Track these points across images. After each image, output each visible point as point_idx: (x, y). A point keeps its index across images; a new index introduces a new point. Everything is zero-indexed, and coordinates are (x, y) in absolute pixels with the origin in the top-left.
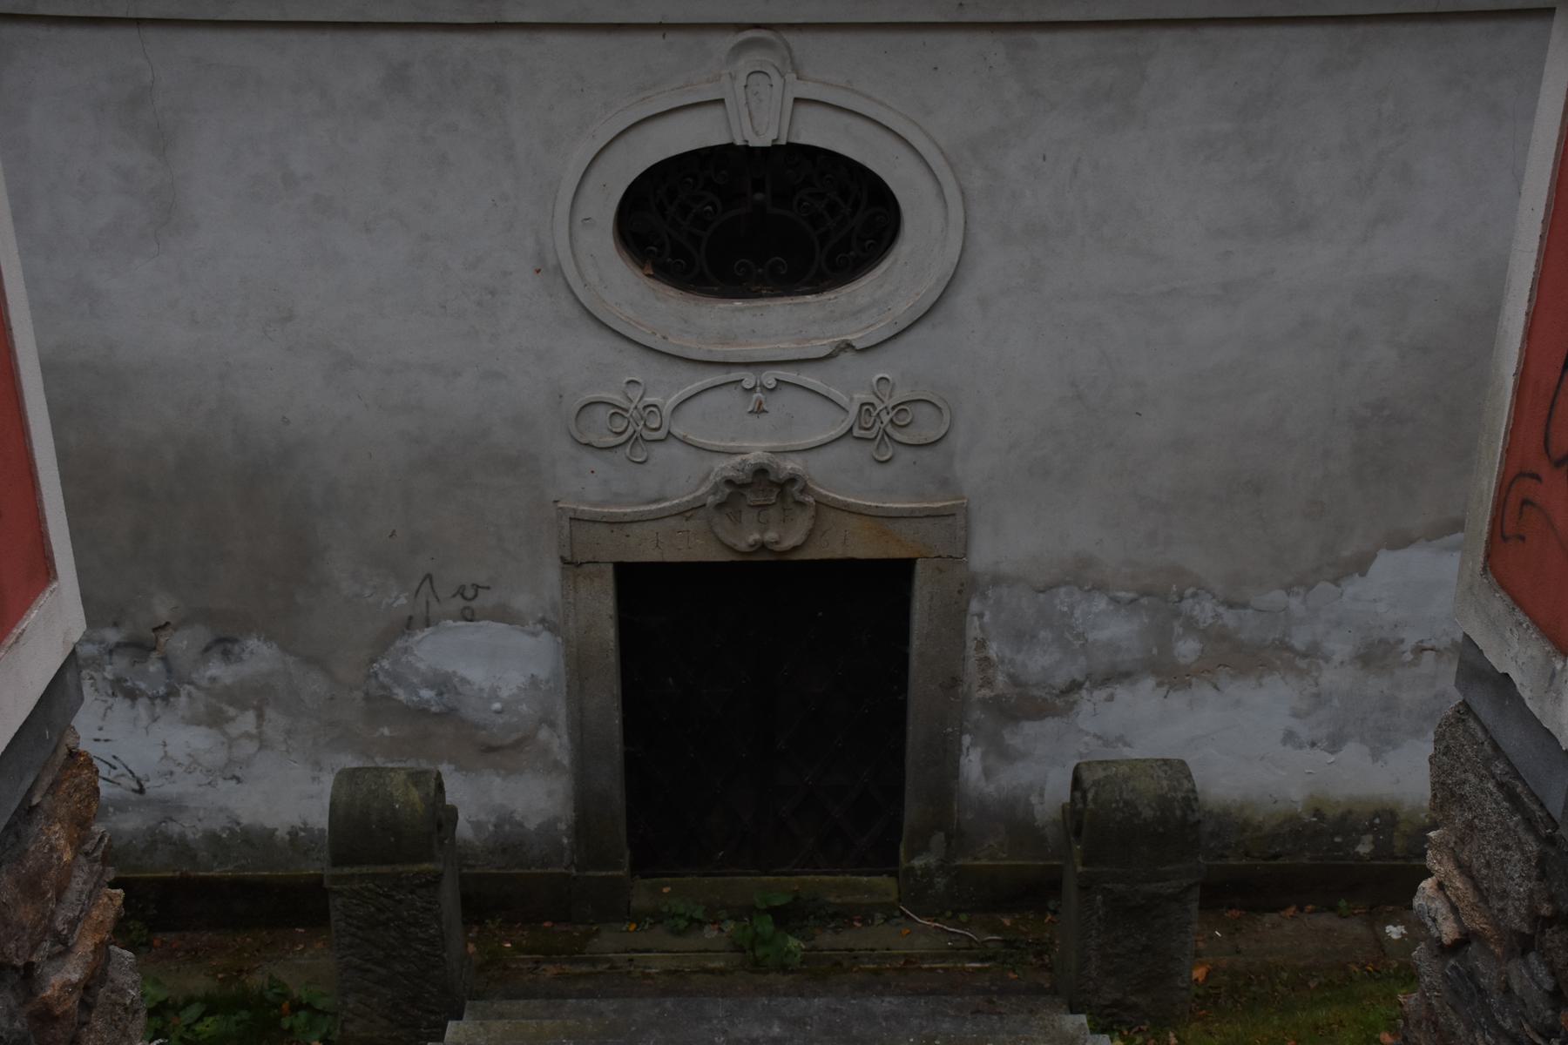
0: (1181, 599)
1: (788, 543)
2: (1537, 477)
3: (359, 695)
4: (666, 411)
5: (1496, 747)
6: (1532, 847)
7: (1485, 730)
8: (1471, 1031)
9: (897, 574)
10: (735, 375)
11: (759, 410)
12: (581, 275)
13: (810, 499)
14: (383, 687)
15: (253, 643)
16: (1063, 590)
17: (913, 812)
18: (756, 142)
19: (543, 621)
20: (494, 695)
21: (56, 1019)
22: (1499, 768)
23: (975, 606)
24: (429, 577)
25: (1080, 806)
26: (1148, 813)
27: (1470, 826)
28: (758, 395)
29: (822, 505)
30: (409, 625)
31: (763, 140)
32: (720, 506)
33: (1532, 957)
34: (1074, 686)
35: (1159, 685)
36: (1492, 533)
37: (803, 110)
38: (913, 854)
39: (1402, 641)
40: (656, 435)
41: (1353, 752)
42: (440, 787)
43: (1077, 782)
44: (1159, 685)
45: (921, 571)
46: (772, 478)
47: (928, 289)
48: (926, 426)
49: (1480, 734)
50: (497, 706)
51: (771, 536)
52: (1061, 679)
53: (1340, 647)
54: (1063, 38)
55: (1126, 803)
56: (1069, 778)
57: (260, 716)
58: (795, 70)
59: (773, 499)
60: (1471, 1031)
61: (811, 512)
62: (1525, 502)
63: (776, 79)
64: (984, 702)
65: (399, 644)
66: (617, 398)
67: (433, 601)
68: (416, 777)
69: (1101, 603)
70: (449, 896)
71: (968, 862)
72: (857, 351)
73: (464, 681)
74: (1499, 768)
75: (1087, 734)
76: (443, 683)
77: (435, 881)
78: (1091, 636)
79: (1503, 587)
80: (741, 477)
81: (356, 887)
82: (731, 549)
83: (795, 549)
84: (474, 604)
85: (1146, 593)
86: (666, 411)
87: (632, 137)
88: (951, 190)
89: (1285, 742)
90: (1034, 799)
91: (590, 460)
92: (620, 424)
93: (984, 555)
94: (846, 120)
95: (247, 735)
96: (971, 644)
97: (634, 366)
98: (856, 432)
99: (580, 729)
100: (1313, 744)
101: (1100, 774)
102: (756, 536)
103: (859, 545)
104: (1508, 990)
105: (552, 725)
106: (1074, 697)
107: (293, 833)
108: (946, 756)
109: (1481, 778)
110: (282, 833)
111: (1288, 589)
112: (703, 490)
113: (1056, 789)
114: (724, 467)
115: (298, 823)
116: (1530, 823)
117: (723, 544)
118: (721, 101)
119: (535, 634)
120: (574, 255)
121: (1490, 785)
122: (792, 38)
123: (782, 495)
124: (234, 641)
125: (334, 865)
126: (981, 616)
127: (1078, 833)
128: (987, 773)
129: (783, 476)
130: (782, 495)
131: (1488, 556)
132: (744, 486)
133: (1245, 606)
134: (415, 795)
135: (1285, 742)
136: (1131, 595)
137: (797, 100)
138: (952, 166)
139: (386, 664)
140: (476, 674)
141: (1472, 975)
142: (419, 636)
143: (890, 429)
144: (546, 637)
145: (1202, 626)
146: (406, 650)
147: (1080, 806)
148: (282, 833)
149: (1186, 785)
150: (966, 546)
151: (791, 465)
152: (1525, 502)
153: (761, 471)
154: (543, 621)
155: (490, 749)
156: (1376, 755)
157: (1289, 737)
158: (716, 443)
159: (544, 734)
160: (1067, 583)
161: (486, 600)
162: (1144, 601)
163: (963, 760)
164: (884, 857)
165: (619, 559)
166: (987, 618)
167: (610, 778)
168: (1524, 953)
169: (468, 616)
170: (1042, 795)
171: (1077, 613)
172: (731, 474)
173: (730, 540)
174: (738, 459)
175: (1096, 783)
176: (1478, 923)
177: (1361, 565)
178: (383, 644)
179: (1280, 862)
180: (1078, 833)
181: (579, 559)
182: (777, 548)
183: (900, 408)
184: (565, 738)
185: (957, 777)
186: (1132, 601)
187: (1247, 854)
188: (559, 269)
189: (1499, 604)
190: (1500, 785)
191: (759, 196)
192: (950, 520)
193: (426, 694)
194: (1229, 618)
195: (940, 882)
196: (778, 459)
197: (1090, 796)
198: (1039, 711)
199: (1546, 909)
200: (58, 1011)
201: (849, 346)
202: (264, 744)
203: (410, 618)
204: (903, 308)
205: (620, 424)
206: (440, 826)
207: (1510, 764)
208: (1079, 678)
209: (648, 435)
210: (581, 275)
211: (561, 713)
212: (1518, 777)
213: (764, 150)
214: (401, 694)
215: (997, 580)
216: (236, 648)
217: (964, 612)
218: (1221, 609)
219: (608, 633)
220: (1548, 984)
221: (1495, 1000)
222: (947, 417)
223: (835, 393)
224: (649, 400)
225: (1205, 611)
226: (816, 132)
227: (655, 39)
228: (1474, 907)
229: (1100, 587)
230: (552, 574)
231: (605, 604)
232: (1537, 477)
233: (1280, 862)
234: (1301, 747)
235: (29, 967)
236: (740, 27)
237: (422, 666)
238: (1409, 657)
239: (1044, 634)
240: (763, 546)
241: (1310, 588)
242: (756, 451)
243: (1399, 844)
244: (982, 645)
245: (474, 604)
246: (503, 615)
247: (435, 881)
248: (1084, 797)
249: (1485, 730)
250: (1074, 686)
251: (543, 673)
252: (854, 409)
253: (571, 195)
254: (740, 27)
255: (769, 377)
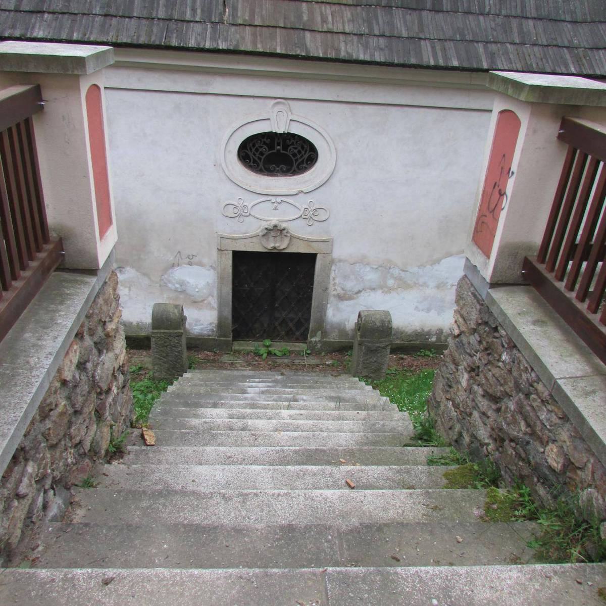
0: (390, 268)
1: (282, 247)
2: (486, 216)
3: (158, 285)
4: (249, 207)
5: (472, 285)
6: (478, 307)
7: (469, 280)
8: (460, 355)
9: (311, 259)
10: (270, 198)
11: (276, 209)
12: (227, 167)
13: (289, 235)
14: (165, 283)
15: (128, 268)
16: (358, 265)
17: (312, 324)
18: (278, 132)
19: (211, 266)
20: (196, 287)
21: (110, 336)
22: (472, 289)
23: (333, 268)
24: (179, 252)
25: (360, 322)
26: (378, 324)
27: (464, 304)
28: (275, 204)
29: (292, 237)
30: (173, 266)
31: (281, 131)
32: (264, 236)
33: (476, 334)
34: (359, 292)
35: (383, 292)
36: (474, 231)
37: (292, 122)
38: (311, 337)
39: (447, 283)
40: (246, 214)
41: (433, 313)
42: (182, 310)
43: (360, 316)
44: (383, 292)
45: (319, 257)
46: (279, 228)
47: (324, 177)
48: (322, 216)
49: (468, 282)
50: (197, 290)
51: (277, 245)
52: (356, 290)
53: (432, 284)
54: (366, 107)
55: (373, 322)
56: (358, 315)
57: (130, 290)
58: (290, 111)
59: (278, 234)
60: (460, 355)
61: (289, 239)
62: (483, 222)
63: (285, 113)
64: (334, 295)
65: (170, 271)
66: (236, 203)
67: (180, 259)
68: (176, 306)
69: (368, 269)
70: (184, 341)
71: (327, 340)
72: (305, 193)
73: (188, 282)
74: (472, 289)
75: (362, 305)
76: (182, 283)
77: (180, 335)
78: (365, 278)
79: (476, 244)
80: (271, 227)
81: (159, 335)
82: (265, 248)
83: (284, 249)
84: (192, 261)
85: (381, 266)
86: (249, 207)
87: (244, 128)
88: (333, 151)
89: (415, 309)
90: (346, 323)
91: (227, 220)
92: (236, 211)
93: (337, 253)
94: (304, 126)
95: (126, 295)
96: (331, 278)
97: (241, 194)
98: (303, 217)
99: (220, 297)
100: (423, 310)
101: (366, 313)
102: (273, 245)
103: (302, 249)
104: (469, 343)
105: (213, 296)
106: (359, 295)
107: (138, 324)
108: (323, 309)
109: (467, 292)
110: (135, 323)
111: (419, 267)
112: (258, 231)
113: (351, 322)
114: (265, 225)
115: (139, 320)
116: (478, 301)
117: (263, 246)
118: (269, 119)
119: (209, 270)
120: (225, 161)
121: (470, 294)
122: (290, 102)
123: (281, 233)
124: (123, 268)
125: (153, 329)
126: (335, 271)
127: (359, 330)
128: (334, 315)
129: (282, 228)
130: (281, 233)
131: (473, 237)
132: (270, 230)
133: (407, 271)
134: (176, 311)
135: (415, 309)
136: (376, 267)
137: (291, 120)
138: (334, 143)
139: (166, 276)
140: (191, 281)
141: (461, 341)
142: (176, 268)
143: (312, 216)
144: (212, 270)
145: (395, 276)
146: (172, 273)
147: (360, 322)
148: (135, 323)
149: (389, 317)
150: (332, 250)
151: (284, 225)
152: (483, 222)
153: (275, 226)
154: (211, 266)
155: (195, 302)
156: (439, 314)
157: (416, 308)
158: (263, 218)
159: (210, 298)
160: (359, 263)
161: (195, 260)
162: (380, 268)
163: (328, 311)
164: (303, 338)
165: (233, 249)
166: (336, 272)
167: (228, 312)
168: (474, 334)
169: (190, 264)
170: (348, 322)
171: (361, 271)
172: (267, 227)
173: (266, 246)
174: (269, 222)
175: (365, 316)
176: (464, 328)
177: (438, 261)
178: (166, 270)
179: (412, 342)
180: (359, 330)
181: (222, 249)
182: (279, 248)
183: (315, 210)
184: (216, 300)
185: (325, 316)
186: (376, 268)
187: (403, 340)
188: (221, 165)
189: (475, 248)
190: (472, 293)
191: (279, 147)
192: (327, 243)
193: (177, 286)
194: (403, 274)
195: (319, 345)
196: (280, 223)
197: (363, 319)
198: (350, 298)
199: (480, 321)
200: (110, 335)
201: (302, 192)
202: (131, 298)
203: (174, 264)
204: (318, 182)
205: (236, 211)
206: (182, 320)
207: (475, 288)
208: (361, 289)
209: (244, 214)
210: (227, 167)
211: (215, 293)
212: (476, 291)
213: (281, 134)
214: (170, 285)
215: (340, 261)
216: (124, 270)
217: (330, 269)
218: (401, 272)
219: (229, 270)
220: (479, 339)
221: (466, 346)
222: (328, 212)
223: (297, 205)
224: (245, 204)
225: (396, 272)
226: (296, 130)
227: (251, 100)
228: (463, 325)
229: (368, 264)
230: (215, 253)
231: (229, 262)
232: (486, 216)
233: (412, 342)
234: (419, 311)
235: (105, 322)
236: (276, 98)
237: (176, 278)
238: (449, 287)
239: (352, 277)
240: (275, 248)
241: (425, 267)
242: (274, 221)
243: (443, 338)
244: (334, 279)
245: (192, 261)
246: (200, 264)
247: (180, 335)
248: (361, 320)
249: (469, 280)
250: (359, 292)
251: (210, 281)
252: (303, 209)
253: (224, 146)
254: (276, 98)
255: (279, 199)
